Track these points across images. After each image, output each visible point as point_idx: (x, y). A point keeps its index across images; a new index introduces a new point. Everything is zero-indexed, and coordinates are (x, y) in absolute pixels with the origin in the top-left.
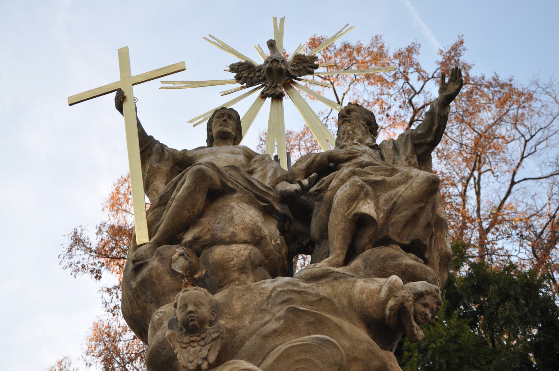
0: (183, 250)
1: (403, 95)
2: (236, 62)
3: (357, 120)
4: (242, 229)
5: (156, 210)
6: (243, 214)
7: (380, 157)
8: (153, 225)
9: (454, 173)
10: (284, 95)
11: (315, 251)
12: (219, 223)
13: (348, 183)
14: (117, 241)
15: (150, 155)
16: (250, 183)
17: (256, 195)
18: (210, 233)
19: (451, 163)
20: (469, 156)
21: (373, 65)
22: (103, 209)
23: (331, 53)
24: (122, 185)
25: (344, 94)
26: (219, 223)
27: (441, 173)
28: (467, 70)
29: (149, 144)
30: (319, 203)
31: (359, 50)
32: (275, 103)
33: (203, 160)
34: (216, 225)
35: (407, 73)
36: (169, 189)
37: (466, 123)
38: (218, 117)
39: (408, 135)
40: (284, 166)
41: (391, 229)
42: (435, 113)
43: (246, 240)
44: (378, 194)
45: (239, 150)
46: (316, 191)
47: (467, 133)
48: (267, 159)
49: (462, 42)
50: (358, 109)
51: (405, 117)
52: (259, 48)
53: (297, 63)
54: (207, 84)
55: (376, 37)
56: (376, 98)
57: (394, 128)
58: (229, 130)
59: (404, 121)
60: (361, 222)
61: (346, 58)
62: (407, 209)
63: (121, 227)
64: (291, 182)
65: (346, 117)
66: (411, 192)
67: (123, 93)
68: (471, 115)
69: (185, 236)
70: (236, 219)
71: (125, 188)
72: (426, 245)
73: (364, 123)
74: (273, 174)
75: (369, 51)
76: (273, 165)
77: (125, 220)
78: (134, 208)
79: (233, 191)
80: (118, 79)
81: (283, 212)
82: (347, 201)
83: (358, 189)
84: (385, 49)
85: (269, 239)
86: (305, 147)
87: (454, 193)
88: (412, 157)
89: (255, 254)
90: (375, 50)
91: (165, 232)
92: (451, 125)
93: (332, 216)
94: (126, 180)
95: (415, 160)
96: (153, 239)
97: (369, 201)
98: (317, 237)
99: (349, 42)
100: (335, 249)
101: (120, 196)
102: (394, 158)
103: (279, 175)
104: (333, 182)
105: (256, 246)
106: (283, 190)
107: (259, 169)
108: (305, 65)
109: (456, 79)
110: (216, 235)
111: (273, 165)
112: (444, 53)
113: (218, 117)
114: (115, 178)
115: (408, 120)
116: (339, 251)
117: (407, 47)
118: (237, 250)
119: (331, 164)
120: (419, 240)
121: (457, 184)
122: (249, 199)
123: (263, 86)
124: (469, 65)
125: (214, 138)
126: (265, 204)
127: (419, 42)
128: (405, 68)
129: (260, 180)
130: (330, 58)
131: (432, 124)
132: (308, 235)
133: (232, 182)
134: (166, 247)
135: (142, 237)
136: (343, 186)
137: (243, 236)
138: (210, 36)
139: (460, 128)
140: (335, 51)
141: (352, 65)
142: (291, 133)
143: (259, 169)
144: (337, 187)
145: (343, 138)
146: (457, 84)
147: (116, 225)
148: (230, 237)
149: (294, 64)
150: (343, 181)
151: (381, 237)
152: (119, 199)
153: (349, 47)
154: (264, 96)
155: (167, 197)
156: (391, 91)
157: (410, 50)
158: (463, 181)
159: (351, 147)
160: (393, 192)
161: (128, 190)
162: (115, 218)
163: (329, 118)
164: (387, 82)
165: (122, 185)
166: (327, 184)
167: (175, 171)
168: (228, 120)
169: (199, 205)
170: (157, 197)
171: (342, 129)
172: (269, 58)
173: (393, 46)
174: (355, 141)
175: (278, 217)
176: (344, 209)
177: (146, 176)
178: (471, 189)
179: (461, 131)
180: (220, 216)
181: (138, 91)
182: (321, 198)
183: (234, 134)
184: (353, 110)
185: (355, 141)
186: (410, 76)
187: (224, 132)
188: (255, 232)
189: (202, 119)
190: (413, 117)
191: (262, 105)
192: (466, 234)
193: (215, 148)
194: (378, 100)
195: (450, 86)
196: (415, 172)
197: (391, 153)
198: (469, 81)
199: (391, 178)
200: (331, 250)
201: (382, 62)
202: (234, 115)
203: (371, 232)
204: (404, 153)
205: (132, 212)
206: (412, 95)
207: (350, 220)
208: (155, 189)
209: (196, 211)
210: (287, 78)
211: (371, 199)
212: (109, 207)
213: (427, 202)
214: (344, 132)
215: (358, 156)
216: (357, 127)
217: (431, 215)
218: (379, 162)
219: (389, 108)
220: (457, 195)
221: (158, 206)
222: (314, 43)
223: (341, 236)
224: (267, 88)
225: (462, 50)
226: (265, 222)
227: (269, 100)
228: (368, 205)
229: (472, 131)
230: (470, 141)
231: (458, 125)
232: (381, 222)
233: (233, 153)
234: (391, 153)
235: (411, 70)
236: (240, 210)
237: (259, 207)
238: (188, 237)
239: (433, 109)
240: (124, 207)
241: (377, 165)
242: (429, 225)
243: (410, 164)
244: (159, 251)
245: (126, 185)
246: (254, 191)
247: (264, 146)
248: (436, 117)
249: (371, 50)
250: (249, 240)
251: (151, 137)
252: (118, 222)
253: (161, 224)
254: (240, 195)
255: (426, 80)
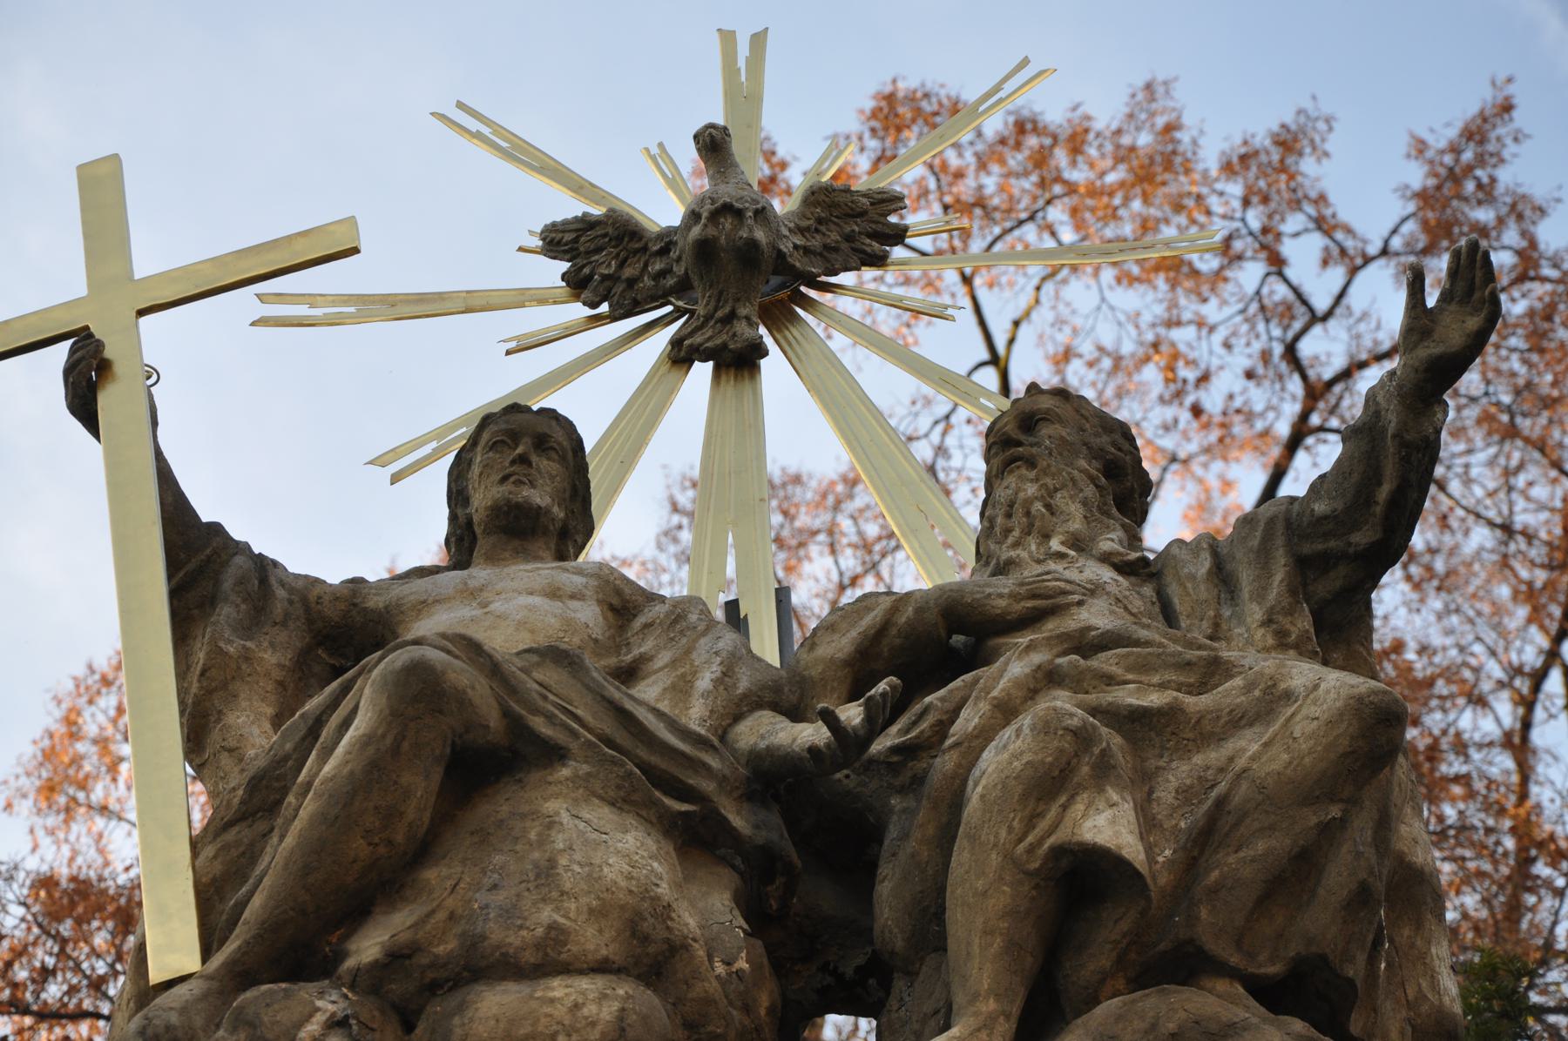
0: (342, 1004)
1: (1261, 327)
2: (570, 215)
3: (1065, 454)
4: (591, 911)
5: (231, 835)
6: (596, 849)
7: (1157, 609)
8: (222, 899)
9: (1478, 648)
10: (765, 353)
11: (893, 1002)
12: (495, 887)
13: (1026, 720)
14: (63, 942)
15: (210, 602)
16: (625, 717)
17: (646, 769)
18: (458, 930)
19: (1466, 607)
20: (1541, 576)
21: (1137, 205)
22: (9, 806)
23: (960, 155)
24: (91, 702)
25: (1017, 324)
26: (495, 887)
27: (1423, 650)
28: (1527, 225)
29: (209, 559)
30: (910, 802)
31: (1076, 142)
32: (729, 387)
33: (426, 626)
34: (482, 897)
35: (1278, 236)
36: (288, 746)
37: (1527, 440)
38: (493, 446)
39: (1271, 521)
40: (766, 645)
41: (1204, 913)
42: (1384, 430)
43: (606, 960)
44: (1152, 763)
45: (579, 580)
46: (895, 750)
47: (1530, 484)
48: (693, 617)
49: (1507, 108)
50: (1064, 410)
51: (1271, 415)
52: (661, 157)
53: (820, 221)
54: (449, 306)
55: (1149, 87)
56: (1150, 337)
57: (1225, 459)
58: (539, 497)
59: (1265, 433)
60: (1083, 879)
61: (1026, 174)
62: (1272, 828)
63: (87, 882)
64: (796, 714)
65: (1019, 444)
66: (1285, 756)
67: (99, 345)
68: (1546, 407)
69: (352, 946)
70: (567, 868)
71: (105, 712)
72: (1351, 982)
73: (1093, 468)
74: (717, 682)
75: (1118, 147)
76: (721, 645)
77: (101, 851)
78: (139, 800)
79: (554, 754)
80: (80, 289)
81: (761, 837)
82: (1025, 797)
83: (1067, 744)
84: (1184, 137)
85: (701, 953)
86: (855, 539)
87: (1477, 737)
88: (1290, 612)
89: (645, 1019)
90: (1144, 139)
91: (271, 928)
92: (1461, 447)
93: (962, 856)
94: (106, 682)
95: (1303, 623)
96: (218, 960)
97: (1115, 797)
98: (899, 944)
99: (1037, 108)
100: (975, 997)
101: (81, 747)
102: (1218, 616)
103: (744, 683)
104: (964, 714)
105: (648, 985)
106: (762, 745)
107: (664, 658)
108: (854, 227)
109: (1470, 291)
110: (483, 937)
111: (721, 645)
112: (1430, 154)
113: (493, 446)
114: (64, 671)
115: (1283, 429)
116: (992, 1005)
117: (1275, 128)
118: (568, 1002)
119: (958, 640)
120: (1323, 958)
121: (1491, 698)
122: (619, 787)
123: (678, 313)
124: (1539, 201)
125: (478, 530)
126: (685, 807)
127: (1326, 108)
128: (1270, 217)
129: (664, 706)
130: (959, 175)
131: (1372, 477)
132: (864, 932)
133: (550, 718)
134: (270, 992)
135: (173, 946)
136: (1008, 732)
137: (594, 940)
138: (461, 105)
139: (1502, 461)
140: (980, 147)
141: (1049, 202)
142: (797, 480)
143: (664, 658)
144: (984, 735)
145: (1007, 531)
146: (1476, 311)
147: (64, 872)
148: (539, 946)
149: (805, 223)
150: (1006, 711)
151: (1162, 947)
152: (77, 760)
153: (1035, 130)
154: (681, 356)
155: (278, 779)
156: (1211, 311)
157: (1288, 142)
158: (1518, 682)
159: (1039, 569)
160: (1212, 756)
161: (114, 721)
162: (57, 843)
163: (953, 419)
164: (1195, 273)
165: (91, 702)
166: (940, 722)
167: (317, 668)
168: (534, 459)
169: (411, 814)
170: (237, 780)
171: (1001, 494)
172: (702, 200)
173: (1218, 126)
174: (1055, 544)
175: (738, 861)
176: (1010, 829)
177: (194, 689)
178: (1552, 716)
179: (1508, 473)
180: (498, 859)
181: (160, 338)
182: (919, 781)
183: (558, 512)
184: (1046, 417)
185: (1055, 544)
186: (1288, 248)
187: (518, 506)
188: (646, 926)
189: (427, 450)
190: (1304, 416)
191: (673, 391)
192: (1533, 909)
193: (479, 574)
194: (1156, 346)
195: (1446, 319)
196: (1302, 673)
197: (1204, 595)
198: (1537, 266)
199: (1204, 701)
200: (959, 999)
201: (1172, 189)
202: (559, 435)
203: (1125, 926)
204: (1259, 595)
205: (132, 816)
206: (1297, 325)
207: (1038, 871)
208: (232, 743)
209: (399, 838)
210: (775, 280)
211: (1121, 788)
212: (32, 797)
213: (1353, 802)
214: (1011, 505)
215: (1069, 606)
216: (1064, 486)
217: (1370, 852)
218: (1152, 632)
219: (1204, 378)
220: (1491, 744)
221: (245, 814)
222: (894, 115)
223: (998, 942)
224: (694, 324)
225: (1509, 141)
226: (687, 879)
227: (703, 371)
228: (1108, 813)
229: (1554, 473)
230: (1544, 516)
231: (1492, 450)
232: (1163, 880)
233: (554, 593)
234: (1204, 595)
235: (1294, 222)
236: (581, 833)
237: (660, 818)
238: (367, 947)
239: (1377, 414)
240: (98, 794)
241: (1147, 643)
242: (1362, 898)
243: (1283, 642)
244: (241, 1009)
245: (108, 701)
246: (643, 753)
247: (686, 536)
248: (1390, 446)
249: (1126, 140)
250: (618, 959)
251: (216, 529)
252: (72, 860)
253: (251, 894)
254: (585, 768)
255: (1356, 264)
